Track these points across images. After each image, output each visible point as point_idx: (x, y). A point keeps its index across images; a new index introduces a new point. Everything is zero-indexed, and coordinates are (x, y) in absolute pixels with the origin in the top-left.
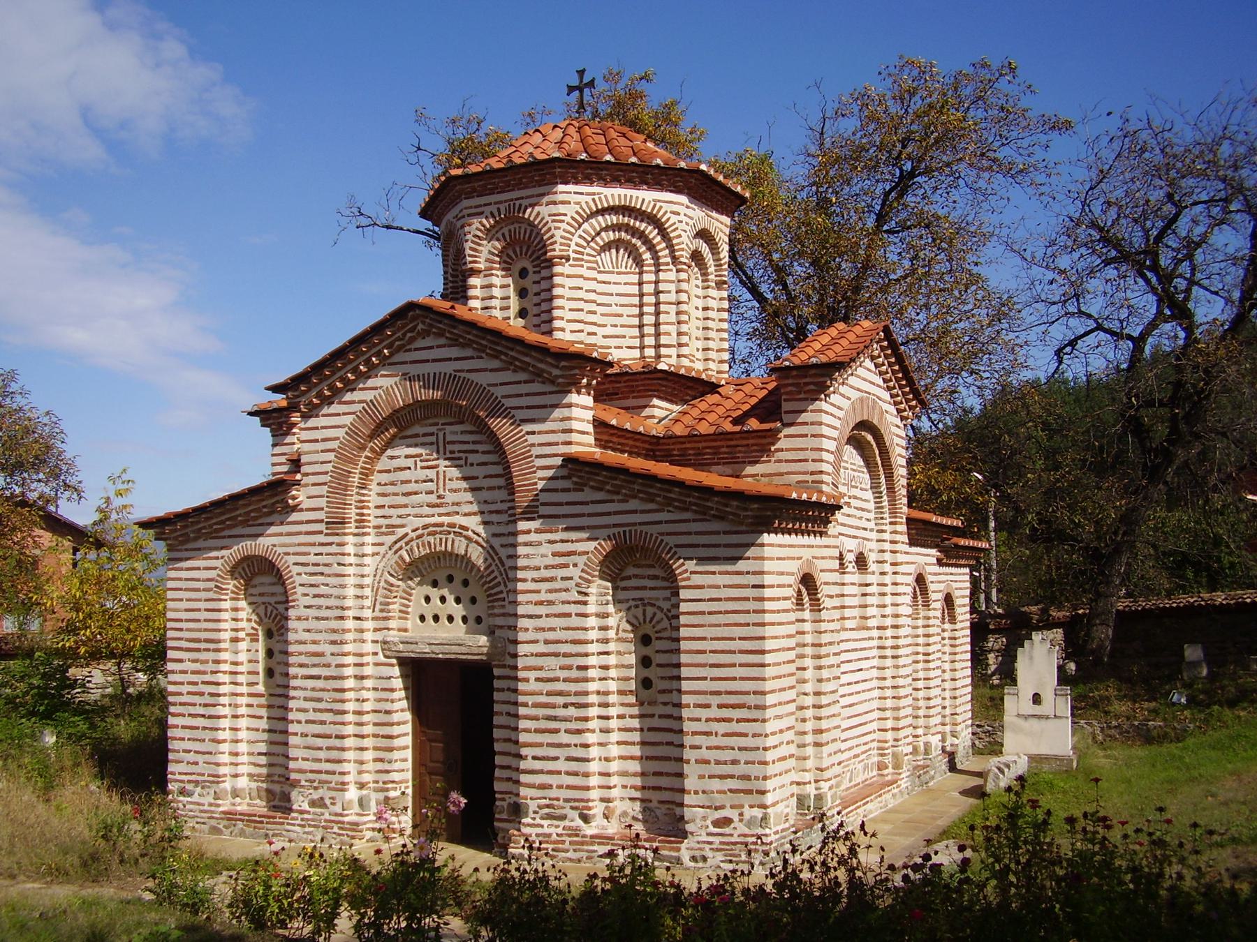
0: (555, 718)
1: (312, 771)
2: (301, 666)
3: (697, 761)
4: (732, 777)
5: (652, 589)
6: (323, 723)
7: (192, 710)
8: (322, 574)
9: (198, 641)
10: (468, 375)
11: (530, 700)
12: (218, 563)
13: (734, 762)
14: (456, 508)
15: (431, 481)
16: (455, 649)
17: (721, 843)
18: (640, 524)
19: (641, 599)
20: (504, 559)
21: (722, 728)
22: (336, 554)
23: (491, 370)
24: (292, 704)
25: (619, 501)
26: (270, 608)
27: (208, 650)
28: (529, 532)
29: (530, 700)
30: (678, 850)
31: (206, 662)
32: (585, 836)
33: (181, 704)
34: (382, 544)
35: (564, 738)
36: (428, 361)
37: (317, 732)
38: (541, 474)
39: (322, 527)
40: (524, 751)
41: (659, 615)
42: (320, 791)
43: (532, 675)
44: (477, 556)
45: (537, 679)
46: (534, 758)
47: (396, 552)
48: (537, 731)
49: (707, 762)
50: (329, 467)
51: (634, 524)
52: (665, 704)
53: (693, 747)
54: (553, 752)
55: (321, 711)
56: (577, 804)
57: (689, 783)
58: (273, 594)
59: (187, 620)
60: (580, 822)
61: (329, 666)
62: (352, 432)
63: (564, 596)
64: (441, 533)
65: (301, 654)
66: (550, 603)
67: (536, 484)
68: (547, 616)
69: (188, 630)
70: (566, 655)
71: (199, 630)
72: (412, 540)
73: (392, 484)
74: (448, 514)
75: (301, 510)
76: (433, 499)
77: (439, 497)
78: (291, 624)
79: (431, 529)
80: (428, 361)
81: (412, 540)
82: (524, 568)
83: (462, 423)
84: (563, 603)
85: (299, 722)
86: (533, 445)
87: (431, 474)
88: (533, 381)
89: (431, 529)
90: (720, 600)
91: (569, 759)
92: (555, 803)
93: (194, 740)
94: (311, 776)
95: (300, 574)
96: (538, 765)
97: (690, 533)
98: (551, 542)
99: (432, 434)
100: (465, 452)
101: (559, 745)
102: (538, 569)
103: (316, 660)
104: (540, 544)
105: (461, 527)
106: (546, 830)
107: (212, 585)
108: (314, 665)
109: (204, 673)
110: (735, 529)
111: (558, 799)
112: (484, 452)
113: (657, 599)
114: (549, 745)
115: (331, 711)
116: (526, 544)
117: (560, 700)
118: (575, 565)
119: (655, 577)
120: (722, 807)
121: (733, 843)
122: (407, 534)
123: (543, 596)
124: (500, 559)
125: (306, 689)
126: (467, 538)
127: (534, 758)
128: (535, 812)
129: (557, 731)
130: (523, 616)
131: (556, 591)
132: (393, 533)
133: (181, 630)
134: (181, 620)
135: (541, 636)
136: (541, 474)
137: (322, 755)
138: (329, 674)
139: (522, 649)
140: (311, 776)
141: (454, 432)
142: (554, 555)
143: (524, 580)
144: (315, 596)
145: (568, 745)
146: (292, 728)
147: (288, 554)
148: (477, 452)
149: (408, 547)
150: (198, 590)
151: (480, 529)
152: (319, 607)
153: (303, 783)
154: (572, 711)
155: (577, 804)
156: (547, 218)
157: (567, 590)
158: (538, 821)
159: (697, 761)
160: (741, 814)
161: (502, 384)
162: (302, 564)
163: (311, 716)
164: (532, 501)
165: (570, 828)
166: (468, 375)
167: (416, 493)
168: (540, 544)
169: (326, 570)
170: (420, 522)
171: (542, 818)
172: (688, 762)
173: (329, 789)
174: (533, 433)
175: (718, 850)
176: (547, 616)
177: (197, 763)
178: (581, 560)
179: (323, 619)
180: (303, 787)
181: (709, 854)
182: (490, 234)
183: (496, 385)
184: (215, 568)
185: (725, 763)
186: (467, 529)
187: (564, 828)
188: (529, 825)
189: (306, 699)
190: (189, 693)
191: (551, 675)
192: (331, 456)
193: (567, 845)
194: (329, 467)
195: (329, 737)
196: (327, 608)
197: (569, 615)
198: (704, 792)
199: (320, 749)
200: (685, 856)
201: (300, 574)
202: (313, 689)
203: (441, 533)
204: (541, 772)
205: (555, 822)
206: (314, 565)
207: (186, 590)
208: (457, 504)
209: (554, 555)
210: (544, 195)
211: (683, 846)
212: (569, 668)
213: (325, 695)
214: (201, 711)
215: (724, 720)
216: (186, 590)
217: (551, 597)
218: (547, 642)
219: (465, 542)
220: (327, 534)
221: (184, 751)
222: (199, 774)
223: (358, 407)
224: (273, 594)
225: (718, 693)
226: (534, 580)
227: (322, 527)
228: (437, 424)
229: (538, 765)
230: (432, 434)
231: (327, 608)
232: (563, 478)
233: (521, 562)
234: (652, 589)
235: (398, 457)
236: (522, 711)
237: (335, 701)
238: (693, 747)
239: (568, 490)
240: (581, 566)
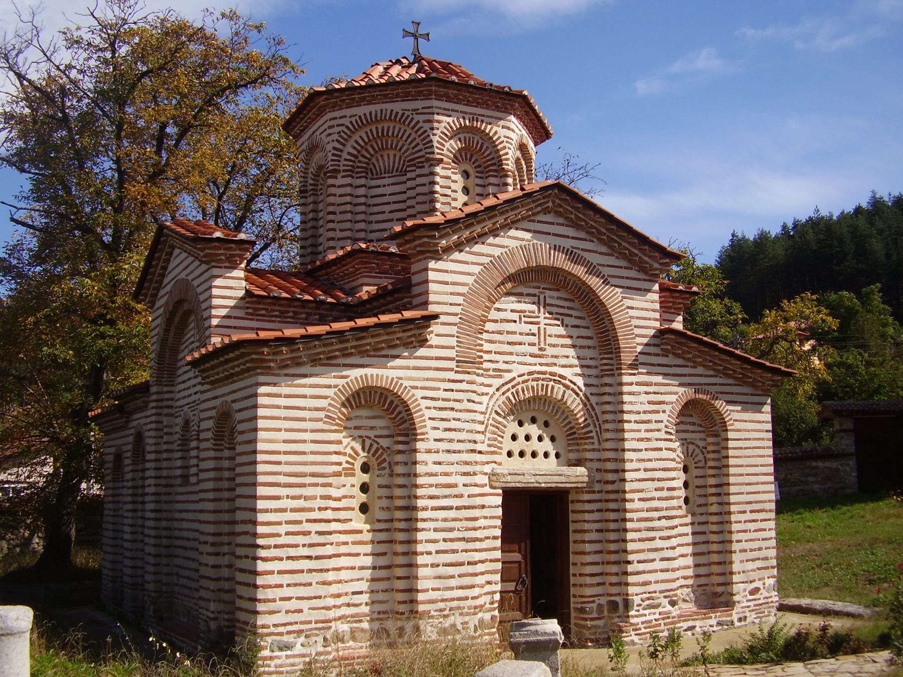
0: (652, 529)
1: (443, 600)
2: (431, 497)
3: (740, 551)
4: (758, 559)
5: (692, 432)
6: (454, 551)
7: (292, 552)
8: (452, 409)
9: (304, 475)
10: (582, 253)
11: (634, 515)
12: (330, 392)
13: (760, 549)
14: (554, 360)
15: (534, 335)
16: (556, 479)
17: (755, 605)
18: (705, 384)
19: (686, 439)
20: (594, 405)
21: (753, 526)
22: (468, 391)
23: (601, 253)
24: (420, 536)
25: (692, 367)
26: (368, 442)
27: (316, 485)
28: (631, 384)
29: (634, 515)
30: (731, 615)
31: (314, 498)
32: (673, 617)
33: (276, 546)
34: (490, 386)
35: (659, 544)
36: (549, 234)
37: (448, 561)
38: (638, 340)
39: (452, 364)
40: (631, 557)
41: (697, 451)
42: (452, 618)
43: (636, 496)
44: (575, 404)
45: (640, 500)
46: (639, 562)
47: (503, 394)
48: (641, 540)
49: (745, 551)
50: (457, 310)
51: (701, 384)
52: (702, 514)
53: (738, 541)
54: (651, 555)
55: (452, 540)
56: (668, 593)
57: (736, 567)
58: (372, 428)
59: (286, 453)
60: (669, 608)
61: (461, 496)
62: (480, 281)
63: (656, 435)
64: (543, 380)
65: (431, 486)
66: (648, 440)
67: (635, 347)
68: (646, 450)
69: (287, 463)
70: (659, 480)
71: (305, 464)
72: (519, 383)
73: (499, 333)
74: (547, 365)
75: (431, 347)
76: (535, 350)
77: (540, 349)
78: (419, 457)
79: (536, 376)
80: (549, 234)
81: (519, 383)
82: (630, 412)
83: (558, 290)
84: (657, 440)
85: (429, 553)
86: (631, 317)
87: (534, 329)
88: (631, 269)
89: (536, 376)
90: (749, 439)
91: (662, 559)
92: (653, 595)
93: (296, 585)
94: (441, 605)
95: (429, 408)
96: (641, 567)
97: (732, 393)
98: (646, 393)
99: (534, 295)
100: (561, 314)
101: (656, 550)
102: (639, 413)
103: (447, 491)
104: (639, 394)
105: (561, 376)
106: (648, 618)
107: (321, 414)
108: (446, 497)
109: (311, 510)
110: (756, 392)
111: (655, 592)
112: (576, 317)
113: (695, 439)
114: (649, 550)
115: (463, 539)
116: (630, 393)
117: (656, 514)
118: (664, 412)
119: (694, 424)
120: (754, 581)
121: (761, 605)
122: (514, 379)
123: (643, 435)
124: (591, 405)
125: (437, 520)
126: (565, 385)
127: (639, 562)
128: (638, 605)
129: (653, 539)
130: (629, 450)
131: (651, 431)
132: (501, 377)
133: (279, 463)
134: (279, 453)
135: (642, 465)
136: (638, 340)
137: (453, 583)
138: (460, 504)
139: (628, 476)
140: (441, 605)
141: (551, 296)
142: (649, 403)
143: (629, 422)
144: (446, 430)
145: (662, 549)
146: (420, 560)
147: (416, 388)
148: (571, 316)
149: (514, 390)
150: (303, 420)
151: (580, 382)
152: (451, 441)
153: (432, 613)
154: (664, 523)
155: (668, 593)
156: (502, 139)
157: (659, 430)
158: (642, 612)
159: (740, 551)
160: (764, 584)
161: (608, 266)
162: (432, 399)
163: (442, 546)
164: (634, 360)
165: (665, 613)
166: (582, 253)
167: (520, 344)
168: (639, 394)
169: (457, 406)
170: (526, 369)
171: (644, 609)
172: (735, 552)
173: (461, 614)
174: (632, 308)
175: (753, 611)
176: (646, 450)
177: (300, 611)
178: (668, 408)
179: (454, 452)
180: (432, 617)
181: (748, 614)
182: (454, 134)
183: (603, 266)
184: (326, 397)
185: (755, 550)
186: (564, 378)
187: (660, 614)
188: (636, 616)
189: (436, 530)
190: (287, 534)
191: (649, 495)
192: (460, 299)
193: (662, 627)
194: (457, 310)
195: (461, 564)
196: (459, 441)
197: (661, 449)
198: (744, 572)
199: (452, 577)
200: (735, 617)
201: (429, 408)
202: (445, 520)
203: (543, 380)
204: (644, 572)
205: (653, 611)
206: (443, 400)
207: (285, 419)
208: (556, 357)
209: (649, 403)
210: (501, 119)
211: (734, 612)
212: (662, 489)
213: (457, 524)
214: (306, 552)
215: (754, 521)
216: (285, 419)
217: (648, 435)
218: (646, 470)
219: (563, 388)
220: (456, 372)
221: (282, 599)
222: (302, 623)
223: (486, 260)
224: (372, 428)
225: (750, 503)
226: (636, 422)
227: (452, 364)
228: (539, 288)
229: (641, 567)
230: (534, 295)
231: (459, 441)
232: (654, 345)
233: (626, 407)
234: (692, 432)
235: (505, 310)
236: (629, 525)
237: (468, 529)
238: (738, 541)
239: (658, 355)
240: (668, 412)
